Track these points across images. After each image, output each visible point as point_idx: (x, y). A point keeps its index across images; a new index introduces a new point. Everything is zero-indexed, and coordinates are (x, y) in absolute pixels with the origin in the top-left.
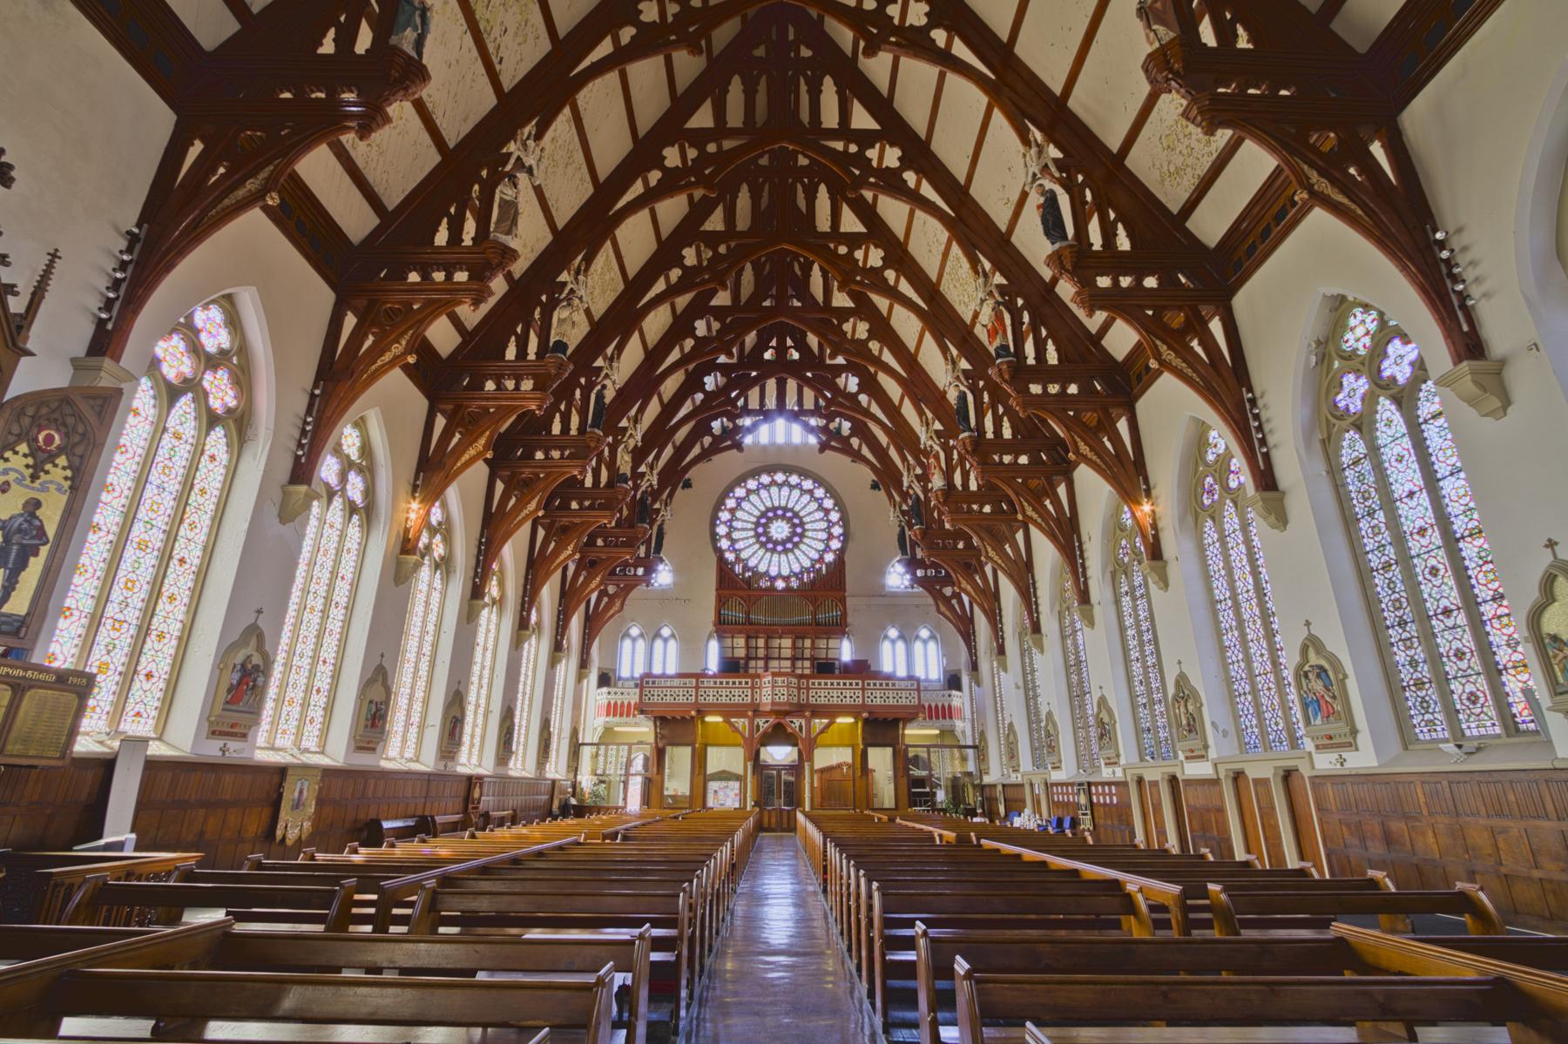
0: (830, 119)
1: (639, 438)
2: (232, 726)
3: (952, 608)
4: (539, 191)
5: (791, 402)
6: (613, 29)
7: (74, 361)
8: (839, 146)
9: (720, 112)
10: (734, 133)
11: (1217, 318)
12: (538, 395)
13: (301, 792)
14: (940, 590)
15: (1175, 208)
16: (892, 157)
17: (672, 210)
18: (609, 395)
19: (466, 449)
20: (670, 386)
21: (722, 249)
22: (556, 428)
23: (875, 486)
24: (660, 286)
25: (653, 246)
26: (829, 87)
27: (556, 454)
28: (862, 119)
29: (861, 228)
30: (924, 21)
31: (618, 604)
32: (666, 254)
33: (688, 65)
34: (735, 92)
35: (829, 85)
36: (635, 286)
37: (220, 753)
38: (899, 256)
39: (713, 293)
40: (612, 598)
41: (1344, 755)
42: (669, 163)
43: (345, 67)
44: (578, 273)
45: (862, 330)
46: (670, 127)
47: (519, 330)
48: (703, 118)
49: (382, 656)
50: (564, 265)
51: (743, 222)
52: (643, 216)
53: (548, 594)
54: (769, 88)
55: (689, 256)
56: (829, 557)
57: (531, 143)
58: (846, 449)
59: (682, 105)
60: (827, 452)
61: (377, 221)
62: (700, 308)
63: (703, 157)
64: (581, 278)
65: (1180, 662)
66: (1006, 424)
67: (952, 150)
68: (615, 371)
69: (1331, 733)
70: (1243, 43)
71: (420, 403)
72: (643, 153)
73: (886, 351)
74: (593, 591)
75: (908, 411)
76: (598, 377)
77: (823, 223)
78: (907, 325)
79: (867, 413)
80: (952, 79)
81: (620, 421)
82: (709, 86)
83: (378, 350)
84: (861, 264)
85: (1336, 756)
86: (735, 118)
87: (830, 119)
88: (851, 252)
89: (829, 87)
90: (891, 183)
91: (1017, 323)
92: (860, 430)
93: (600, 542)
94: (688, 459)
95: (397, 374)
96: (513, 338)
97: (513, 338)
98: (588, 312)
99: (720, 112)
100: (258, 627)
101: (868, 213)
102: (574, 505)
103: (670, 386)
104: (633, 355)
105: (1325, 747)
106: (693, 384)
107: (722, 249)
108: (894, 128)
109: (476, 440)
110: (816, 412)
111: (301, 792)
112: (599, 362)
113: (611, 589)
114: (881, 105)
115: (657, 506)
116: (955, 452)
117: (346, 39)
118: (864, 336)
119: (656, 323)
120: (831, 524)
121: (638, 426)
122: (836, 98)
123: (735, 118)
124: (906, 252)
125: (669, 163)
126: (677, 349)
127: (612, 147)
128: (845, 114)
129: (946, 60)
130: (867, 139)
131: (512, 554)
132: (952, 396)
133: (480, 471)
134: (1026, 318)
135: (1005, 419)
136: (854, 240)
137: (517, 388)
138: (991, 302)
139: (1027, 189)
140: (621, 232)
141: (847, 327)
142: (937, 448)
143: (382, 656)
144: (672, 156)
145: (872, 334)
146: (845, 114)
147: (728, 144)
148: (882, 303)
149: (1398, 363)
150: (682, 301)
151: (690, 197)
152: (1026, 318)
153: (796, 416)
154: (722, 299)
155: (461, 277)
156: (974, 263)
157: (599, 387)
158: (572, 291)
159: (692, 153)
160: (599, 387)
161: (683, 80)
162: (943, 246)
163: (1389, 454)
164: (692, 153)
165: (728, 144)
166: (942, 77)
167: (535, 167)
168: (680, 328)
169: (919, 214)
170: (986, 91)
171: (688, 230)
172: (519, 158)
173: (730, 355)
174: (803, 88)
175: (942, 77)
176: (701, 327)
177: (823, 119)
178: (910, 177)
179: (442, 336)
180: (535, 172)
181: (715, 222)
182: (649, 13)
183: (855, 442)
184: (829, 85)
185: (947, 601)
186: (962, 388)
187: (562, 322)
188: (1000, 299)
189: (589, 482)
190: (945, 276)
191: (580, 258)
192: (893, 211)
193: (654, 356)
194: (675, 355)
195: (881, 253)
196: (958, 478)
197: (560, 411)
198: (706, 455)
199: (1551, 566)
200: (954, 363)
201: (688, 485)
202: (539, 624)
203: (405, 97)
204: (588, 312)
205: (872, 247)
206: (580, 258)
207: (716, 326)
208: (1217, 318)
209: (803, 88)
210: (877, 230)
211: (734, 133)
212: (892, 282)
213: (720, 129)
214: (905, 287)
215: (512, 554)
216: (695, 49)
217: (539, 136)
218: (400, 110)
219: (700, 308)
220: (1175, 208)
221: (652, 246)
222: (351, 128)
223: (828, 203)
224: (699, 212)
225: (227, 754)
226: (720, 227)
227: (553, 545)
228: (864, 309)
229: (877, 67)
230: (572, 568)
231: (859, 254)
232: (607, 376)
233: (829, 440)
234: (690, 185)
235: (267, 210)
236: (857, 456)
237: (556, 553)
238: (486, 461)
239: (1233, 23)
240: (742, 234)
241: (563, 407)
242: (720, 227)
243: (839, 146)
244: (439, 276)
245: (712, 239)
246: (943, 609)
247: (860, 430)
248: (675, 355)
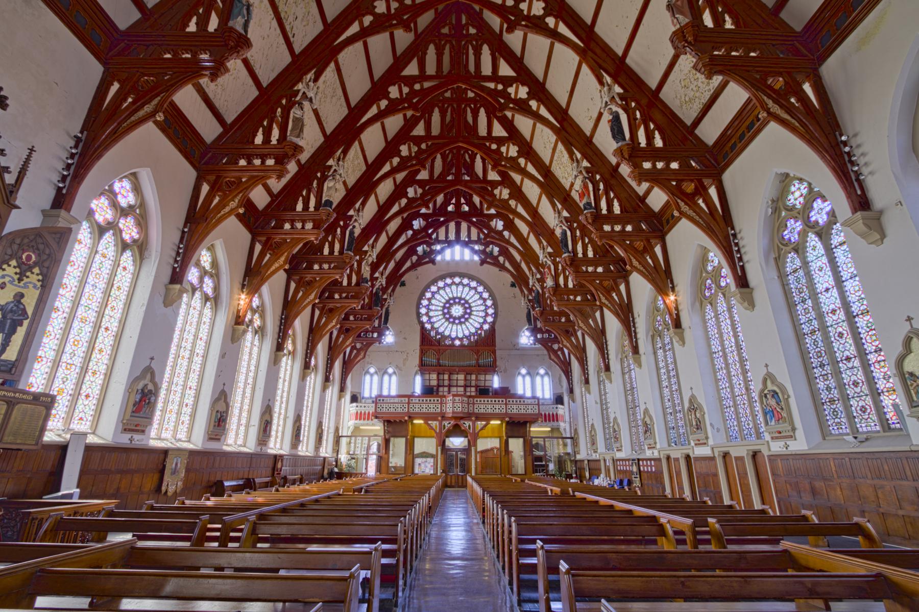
0: (487, 70)
1: (375, 257)
2: (136, 426)
3: (558, 357)
4: (316, 112)
5: (464, 236)
6: (359, 16)
7: (43, 211)
8: (492, 85)
9: (422, 65)
10: (430, 78)
11: (713, 187)
12: (316, 231)
13: (176, 464)
14: (551, 346)
15: (689, 122)
16: (523, 92)
17: (394, 123)
18: (357, 232)
19: (273, 263)
20: (393, 227)
21: (423, 146)
22: (326, 251)
23: (513, 285)
24: (387, 168)
25: (383, 145)
26: (486, 51)
27: (326, 266)
28: (505, 70)
29: (497, 178)
30: (541, 12)
31: (362, 354)
32: (390, 149)
33: (404, 38)
34: (436, 117)
35: (486, 50)
36: (372, 168)
37: (129, 442)
38: (527, 150)
39: (418, 171)
40: (359, 351)
41: (788, 443)
42: (393, 96)
43: (202, 39)
44: (339, 160)
45: (505, 193)
46: (393, 75)
47: (304, 193)
48: (412, 69)
49: (224, 384)
50: (330, 155)
51: (436, 130)
52: (376, 127)
53: (321, 348)
54: (451, 52)
55: (404, 150)
56: (486, 327)
57: (311, 84)
58: (496, 263)
59: (400, 62)
60: (485, 265)
61: (221, 130)
62: (410, 180)
63: (413, 93)
64: (341, 163)
65: (691, 388)
66: (590, 249)
67: (558, 88)
68: (360, 218)
69: (780, 430)
70: (729, 25)
71: (246, 236)
72: (377, 90)
73: (519, 206)
74: (347, 346)
75: (532, 241)
76: (350, 221)
77: (483, 131)
78: (531, 190)
79: (508, 242)
80: (558, 46)
81: (363, 247)
82: (416, 50)
83: (306, 296)
84: (504, 155)
85: (783, 443)
86: (431, 69)
87: (487, 70)
88: (499, 148)
89: (486, 51)
90: (522, 107)
91: (596, 189)
92: (504, 252)
93: (352, 318)
94: (404, 269)
95: (233, 219)
96: (261, 129)
97: (327, 243)
98: (345, 183)
99: (422, 65)
100: (151, 368)
101: (509, 125)
102: (337, 296)
103: (393, 227)
104: (371, 208)
105: (777, 438)
106: (406, 225)
107: (423, 146)
108: (524, 75)
109: (278, 258)
110: (478, 241)
111: (176, 464)
112: (351, 213)
113: (358, 346)
114: (517, 62)
115: (385, 297)
116: (560, 265)
117: (203, 23)
118: (507, 197)
119: (385, 189)
120: (487, 307)
121: (374, 250)
122: (486, 119)
123: (431, 69)
124: (531, 148)
125: (378, 10)
126: (397, 205)
127: (359, 87)
128: (495, 67)
129: (554, 35)
130: (507, 82)
131: (300, 325)
132: (558, 232)
133: (281, 276)
134: (601, 186)
135: (589, 245)
136: (500, 141)
137: (303, 228)
138: (581, 177)
139: (602, 111)
140: (364, 136)
141: (497, 192)
142: (549, 263)
143: (224, 384)
144: (394, 92)
145: (511, 196)
146: (495, 67)
147: (427, 85)
148: (517, 178)
149: (820, 213)
150: (400, 177)
151: (405, 116)
152: (601, 186)
153: (466, 244)
154: (423, 175)
155: (270, 162)
156: (571, 155)
157: (351, 227)
158: (335, 171)
159: (406, 90)
160: (351, 227)
161: (401, 48)
162: (553, 145)
163: (814, 266)
164: (406, 90)
165: (427, 85)
166: (534, 126)
167: (313, 98)
168: (399, 192)
169: (539, 125)
170: (578, 53)
171: (404, 135)
172: (304, 93)
173: (428, 208)
174: (471, 51)
175: (534, 126)
176: (411, 192)
177: (482, 70)
178: (533, 104)
179: (259, 197)
180: (314, 101)
181: (419, 130)
182: (381, 8)
183: (501, 259)
184: (486, 50)
185: (555, 352)
186: (564, 228)
187: (329, 189)
188: (586, 175)
189: (345, 283)
190: (554, 162)
191: (340, 151)
192: (523, 124)
193: (383, 209)
194: (395, 208)
195: (516, 148)
196: (561, 280)
197: (328, 241)
198: (414, 267)
199: (910, 332)
200: (559, 213)
201: (403, 284)
202: (316, 366)
203: (237, 57)
204: (345, 183)
205: (511, 145)
206: (340, 151)
207: (420, 191)
208: (713, 187)
209: (471, 51)
210: (514, 135)
211: (430, 78)
212: (523, 166)
213: (423, 76)
214: (531, 169)
215: (300, 325)
216: (407, 29)
217: (316, 80)
218: (235, 65)
219: (410, 180)
220: (689, 122)
221: (368, 85)
222: (206, 75)
223: (490, 58)
224: (410, 124)
225: (133, 442)
226: (427, 177)
227: (324, 320)
228: (506, 181)
229: (514, 40)
230: (335, 333)
231: (503, 149)
232: (356, 220)
233: (486, 258)
234: (404, 108)
235: (156, 123)
236: (502, 267)
237: (326, 324)
238: (285, 270)
239: (723, 13)
240: (435, 138)
241: (330, 239)
242: (427, 177)
243: (492, 85)
244: (257, 162)
245: (417, 140)
246: (553, 357)
247: (504, 252)
248: (395, 208)
